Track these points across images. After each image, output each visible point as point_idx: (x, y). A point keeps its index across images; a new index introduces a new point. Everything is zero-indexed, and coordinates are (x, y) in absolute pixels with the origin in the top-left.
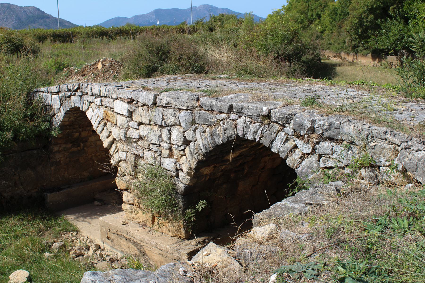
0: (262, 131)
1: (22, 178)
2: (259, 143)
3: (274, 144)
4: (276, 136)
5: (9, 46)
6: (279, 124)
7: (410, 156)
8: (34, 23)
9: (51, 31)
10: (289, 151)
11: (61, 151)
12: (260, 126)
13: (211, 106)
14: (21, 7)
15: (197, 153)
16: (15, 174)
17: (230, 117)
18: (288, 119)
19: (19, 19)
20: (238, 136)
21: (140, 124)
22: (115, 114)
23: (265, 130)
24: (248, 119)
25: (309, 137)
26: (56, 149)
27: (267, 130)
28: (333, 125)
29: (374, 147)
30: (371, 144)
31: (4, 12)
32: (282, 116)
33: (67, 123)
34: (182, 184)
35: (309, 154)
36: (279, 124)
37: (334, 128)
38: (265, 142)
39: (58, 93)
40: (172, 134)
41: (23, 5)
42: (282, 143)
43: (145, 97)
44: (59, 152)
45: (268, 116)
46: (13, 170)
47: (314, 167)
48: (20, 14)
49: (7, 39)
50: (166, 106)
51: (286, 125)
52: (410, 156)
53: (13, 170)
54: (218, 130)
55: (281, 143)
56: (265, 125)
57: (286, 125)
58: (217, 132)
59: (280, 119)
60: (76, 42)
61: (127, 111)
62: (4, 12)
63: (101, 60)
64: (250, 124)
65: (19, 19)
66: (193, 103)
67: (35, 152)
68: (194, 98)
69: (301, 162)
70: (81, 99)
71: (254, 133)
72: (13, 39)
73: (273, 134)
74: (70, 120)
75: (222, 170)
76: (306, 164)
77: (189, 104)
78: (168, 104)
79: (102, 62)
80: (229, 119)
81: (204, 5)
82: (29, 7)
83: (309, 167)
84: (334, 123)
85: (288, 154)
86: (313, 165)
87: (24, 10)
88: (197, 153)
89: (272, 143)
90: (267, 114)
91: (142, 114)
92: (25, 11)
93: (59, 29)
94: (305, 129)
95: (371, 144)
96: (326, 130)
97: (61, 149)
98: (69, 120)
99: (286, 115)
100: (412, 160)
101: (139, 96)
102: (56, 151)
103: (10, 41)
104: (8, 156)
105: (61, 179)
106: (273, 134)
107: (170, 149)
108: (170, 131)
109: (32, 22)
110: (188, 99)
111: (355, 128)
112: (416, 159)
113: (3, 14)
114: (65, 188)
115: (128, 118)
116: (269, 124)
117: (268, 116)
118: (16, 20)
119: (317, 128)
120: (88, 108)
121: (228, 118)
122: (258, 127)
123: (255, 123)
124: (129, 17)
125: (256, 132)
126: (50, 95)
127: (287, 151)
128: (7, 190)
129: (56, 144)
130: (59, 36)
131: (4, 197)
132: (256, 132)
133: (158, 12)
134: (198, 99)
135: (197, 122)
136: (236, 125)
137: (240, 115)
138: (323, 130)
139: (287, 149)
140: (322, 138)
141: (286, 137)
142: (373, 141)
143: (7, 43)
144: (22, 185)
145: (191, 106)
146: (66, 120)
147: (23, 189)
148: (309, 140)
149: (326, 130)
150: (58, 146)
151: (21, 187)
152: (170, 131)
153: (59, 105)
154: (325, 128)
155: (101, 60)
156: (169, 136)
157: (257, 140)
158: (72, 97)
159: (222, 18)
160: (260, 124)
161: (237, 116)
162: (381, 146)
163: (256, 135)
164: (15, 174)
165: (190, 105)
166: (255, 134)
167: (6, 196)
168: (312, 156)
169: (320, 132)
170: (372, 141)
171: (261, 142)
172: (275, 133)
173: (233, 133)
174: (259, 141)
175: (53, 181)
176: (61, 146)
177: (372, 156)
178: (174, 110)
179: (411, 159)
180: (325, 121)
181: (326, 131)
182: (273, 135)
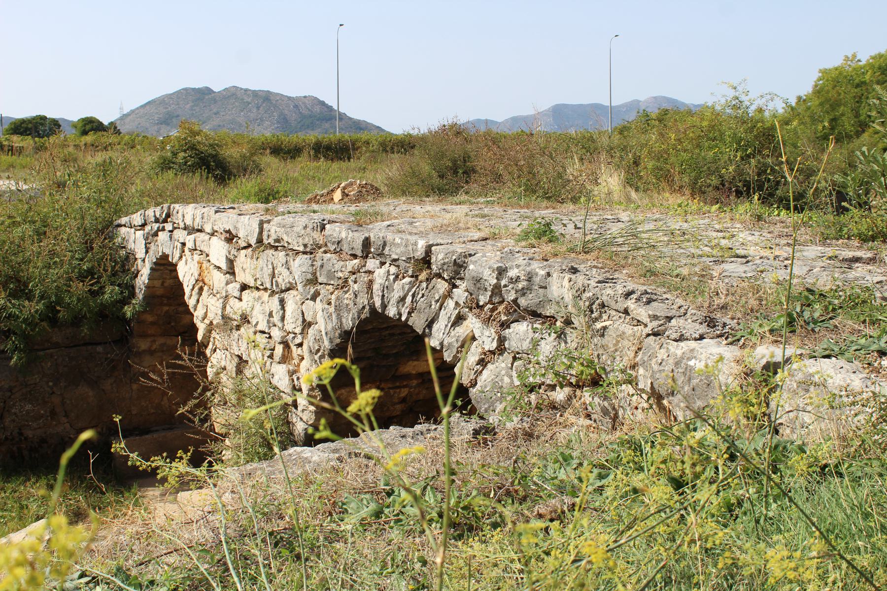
0: (413, 296)
1: (68, 402)
2: (405, 324)
3: (435, 327)
4: (440, 309)
5: (190, 156)
6: (444, 279)
7: (662, 354)
8: (313, 130)
9: (312, 136)
10: (459, 344)
11: (155, 351)
12: (412, 284)
13: (339, 242)
14: (289, 98)
15: (318, 351)
16: (53, 393)
17: (365, 266)
18: (459, 266)
19: (284, 121)
20: (373, 310)
21: (244, 287)
22: (212, 267)
23: (420, 295)
24: (393, 270)
25: (492, 310)
26: (143, 345)
27: (423, 296)
28: (534, 279)
29: (603, 331)
30: (599, 325)
31: (258, 108)
32: (446, 260)
33: (160, 292)
34: (302, 423)
35: (493, 352)
36: (444, 279)
37: (536, 287)
38: (418, 323)
39: (143, 226)
40: (286, 308)
41: (293, 95)
42: (450, 325)
43: (248, 228)
44: (151, 352)
45: (426, 261)
46: (51, 384)
47: (504, 385)
48: (286, 112)
49: (186, 144)
50: (277, 244)
51: (458, 282)
52: (662, 354)
53: (51, 384)
54: (347, 296)
55: (446, 326)
56: (421, 282)
57: (458, 282)
58: (345, 301)
59: (445, 267)
60: (359, 158)
61: (224, 261)
62: (258, 108)
63: (343, 185)
64: (395, 280)
65: (284, 121)
66: (315, 236)
67: (100, 349)
68: (315, 225)
69: (481, 372)
70: (171, 237)
71: (398, 303)
72: (199, 142)
73: (433, 303)
74: (166, 284)
75: (403, 400)
76: (489, 376)
77: (306, 241)
78: (277, 240)
79: (344, 188)
80: (364, 269)
81: (655, 98)
82: (305, 97)
83: (494, 383)
84: (537, 274)
85: (458, 352)
86: (502, 380)
87: (296, 103)
88: (318, 351)
89: (430, 325)
90: (423, 255)
91: (248, 268)
92: (296, 106)
93: (336, 134)
94: (486, 290)
95: (599, 325)
96: (523, 292)
97: (154, 347)
98: (162, 284)
99: (454, 257)
100: (664, 363)
101: (239, 225)
102: (144, 351)
103: (193, 147)
104: (42, 353)
105: (152, 411)
106: (433, 303)
107: (286, 345)
108: (282, 302)
109: (308, 127)
110: (305, 227)
111: (572, 283)
112: (671, 361)
113: (255, 110)
114: (156, 431)
115: (228, 275)
116: (428, 280)
117: (426, 261)
118: (278, 122)
119: (505, 286)
120: (181, 257)
121: (362, 267)
122: (407, 287)
123: (404, 277)
124: (500, 121)
125: (402, 300)
126: (133, 230)
127: (456, 345)
128: (35, 425)
129: (144, 336)
130: (328, 148)
131: (26, 439)
132: (402, 300)
133: (559, 111)
134: (323, 228)
135: (320, 281)
136: (371, 282)
137: (383, 260)
138: (517, 291)
139: (457, 341)
140: (517, 313)
141: (457, 311)
142: (605, 317)
143: (185, 151)
144: (66, 416)
145: (311, 242)
146: (158, 283)
147: (68, 425)
148: (491, 316)
149: (523, 292)
150: (149, 340)
151: (64, 420)
152: (282, 302)
153: (144, 251)
154: (520, 286)
155: (343, 185)
156: (281, 312)
157: (403, 319)
158: (160, 233)
159: (664, 117)
160: (413, 279)
161: (378, 262)
162: (617, 329)
163: (403, 306)
164: (53, 393)
165: (308, 241)
166: (401, 305)
167: (31, 436)
168: (501, 357)
169: (511, 296)
170: (601, 316)
171: (410, 323)
172: (437, 301)
173: (366, 302)
174: (407, 320)
175: (134, 412)
176: (154, 341)
177: (598, 355)
178: (287, 255)
179: (663, 360)
180: (521, 268)
181: (524, 295)
182: (433, 307)
